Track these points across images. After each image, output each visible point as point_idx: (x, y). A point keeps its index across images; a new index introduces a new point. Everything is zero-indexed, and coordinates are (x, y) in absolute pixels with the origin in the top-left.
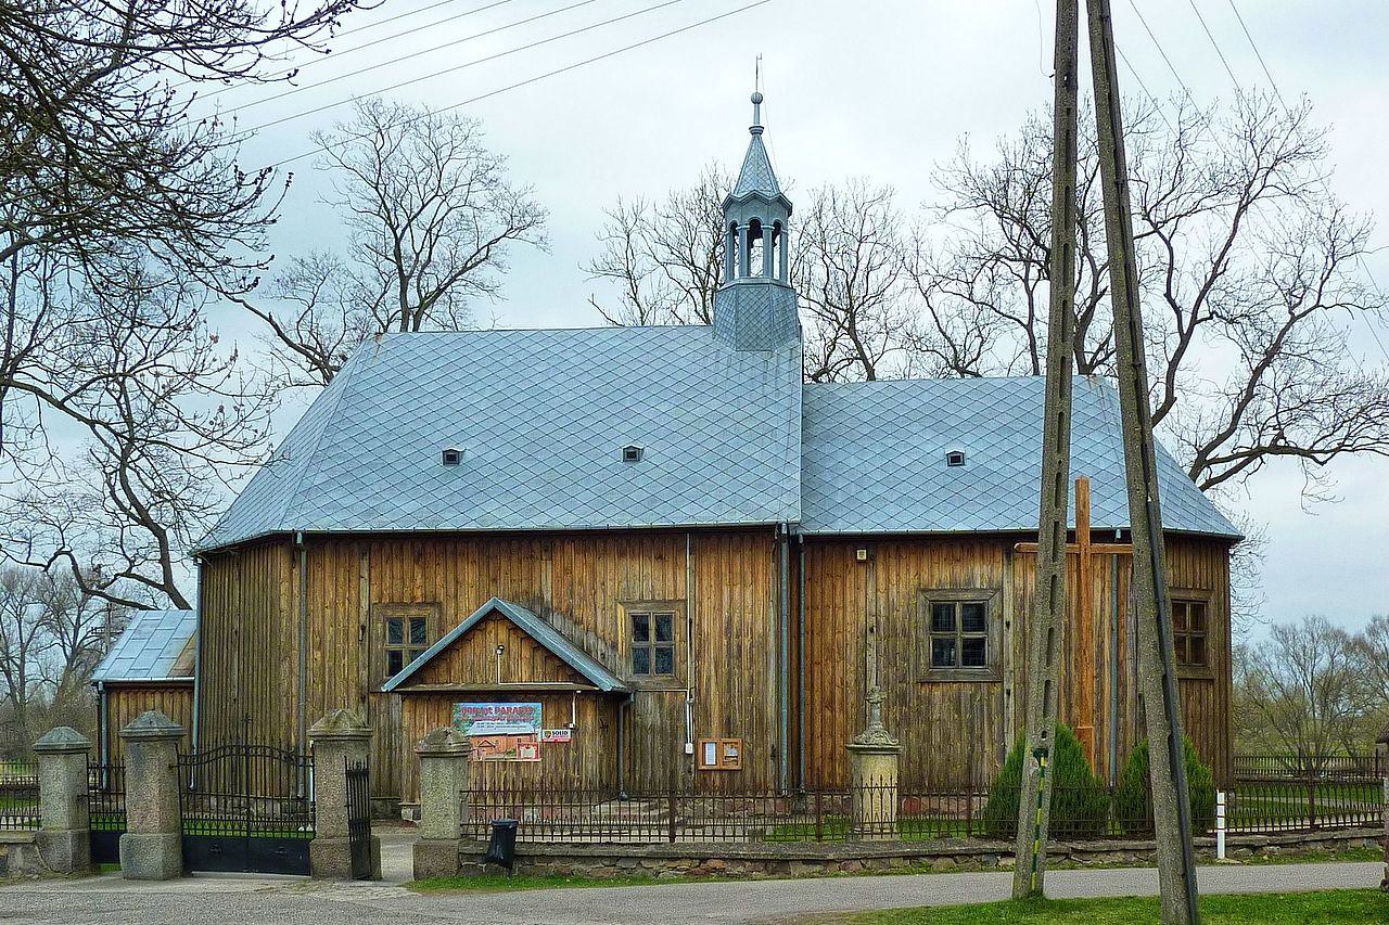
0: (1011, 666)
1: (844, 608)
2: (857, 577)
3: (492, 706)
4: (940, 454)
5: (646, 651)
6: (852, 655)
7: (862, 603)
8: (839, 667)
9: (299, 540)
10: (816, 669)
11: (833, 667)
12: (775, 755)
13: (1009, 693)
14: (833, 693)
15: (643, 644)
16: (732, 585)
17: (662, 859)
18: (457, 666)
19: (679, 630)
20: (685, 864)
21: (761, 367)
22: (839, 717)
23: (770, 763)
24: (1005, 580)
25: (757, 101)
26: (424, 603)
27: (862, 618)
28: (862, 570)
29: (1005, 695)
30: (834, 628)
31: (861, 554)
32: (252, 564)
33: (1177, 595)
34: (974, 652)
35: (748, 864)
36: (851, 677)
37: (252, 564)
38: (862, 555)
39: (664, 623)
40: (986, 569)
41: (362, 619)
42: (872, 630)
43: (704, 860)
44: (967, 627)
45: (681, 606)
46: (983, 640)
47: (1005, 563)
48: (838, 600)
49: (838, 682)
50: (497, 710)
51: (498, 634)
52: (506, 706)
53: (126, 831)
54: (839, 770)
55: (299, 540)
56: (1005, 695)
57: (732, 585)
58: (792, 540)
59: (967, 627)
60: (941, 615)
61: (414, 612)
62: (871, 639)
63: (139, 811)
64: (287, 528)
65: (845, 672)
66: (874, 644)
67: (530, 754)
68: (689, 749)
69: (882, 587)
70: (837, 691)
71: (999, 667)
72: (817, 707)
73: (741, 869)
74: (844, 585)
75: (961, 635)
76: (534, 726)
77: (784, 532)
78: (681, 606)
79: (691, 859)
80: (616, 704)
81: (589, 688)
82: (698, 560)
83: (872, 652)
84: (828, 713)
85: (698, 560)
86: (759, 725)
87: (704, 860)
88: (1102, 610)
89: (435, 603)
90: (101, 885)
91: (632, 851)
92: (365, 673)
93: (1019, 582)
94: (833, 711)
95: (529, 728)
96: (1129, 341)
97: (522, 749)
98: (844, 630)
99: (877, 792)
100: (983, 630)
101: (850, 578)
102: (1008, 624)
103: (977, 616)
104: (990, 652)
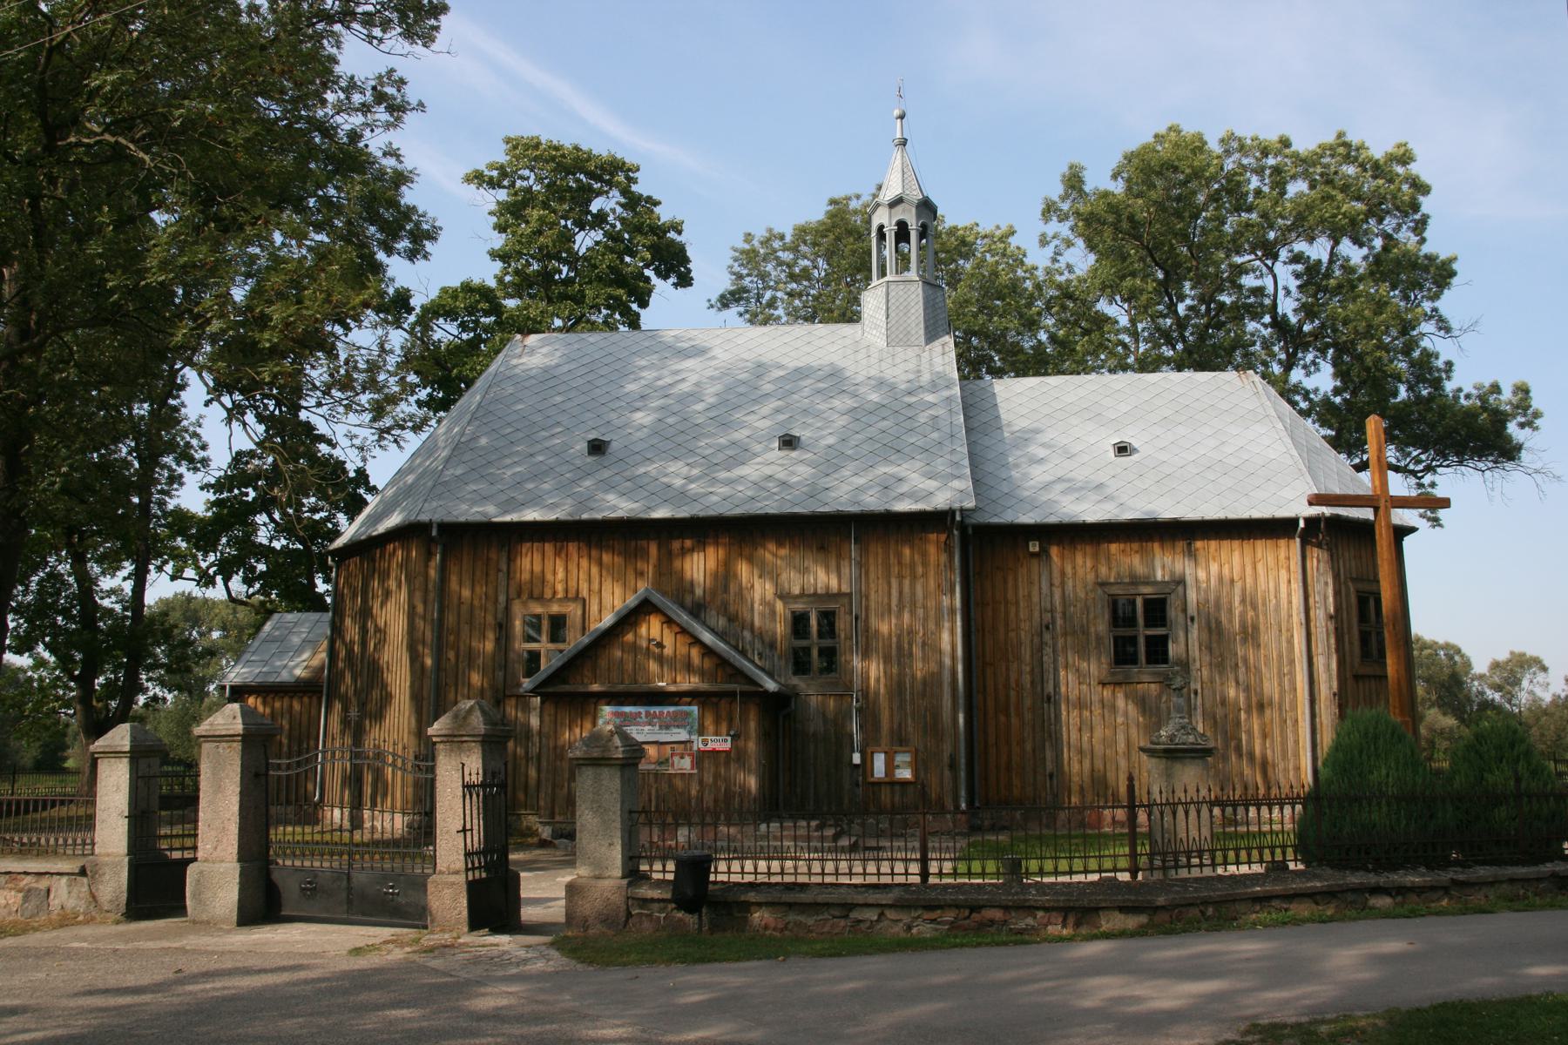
0: (1198, 664)
1: (1017, 603)
2: (1029, 571)
3: (642, 710)
5: (807, 650)
6: (1026, 654)
7: (1035, 599)
9: (434, 533)
10: (989, 671)
11: (1008, 669)
12: (953, 766)
14: (1008, 697)
15: (804, 643)
16: (901, 577)
17: (916, 908)
18: (603, 663)
19: (843, 624)
20: (949, 916)
21: (914, 361)
22: (1014, 720)
23: (947, 773)
26: (566, 598)
27: (1036, 614)
28: (1035, 562)
30: (1007, 625)
33: (1360, 586)
34: (1158, 651)
35: (1040, 914)
36: (1027, 679)
38: (1034, 547)
39: (828, 618)
40: (1168, 560)
41: (500, 616)
43: (975, 908)
44: (1149, 623)
45: (846, 600)
48: (1010, 595)
50: (648, 714)
51: (892, 286)
52: (657, 710)
53: (195, 859)
54: (1016, 782)
55: (434, 533)
57: (901, 577)
58: (963, 527)
59: (1149, 623)
60: (1121, 615)
61: (555, 609)
63: (213, 833)
64: (424, 518)
65: (1020, 673)
67: (685, 764)
68: (857, 758)
70: (1013, 694)
71: (1185, 665)
73: (1030, 921)
74: (1016, 580)
75: (1143, 632)
76: (690, 733)
77: (958, 518)
78: (846, 600)
79: (957, 907)
80: (778, 708)
81: (753, 688)
82: (864, 550)
84: (1002, 719)
85: (864, 550)
86: (932, 727)
87: (975, 908)
88: (1290, 602)
89: (577, 597)
90: (151, 936)
91: (873, 897)
92: (501, 674)
94: (1008, 716)
95: (683, 735)
97: (676, 759)
98: (1018, 628)
99: (1192, 808)
101: (1023, 572)
102: (1192, 619)
103: (1157, 610)
104: (1174, 650)
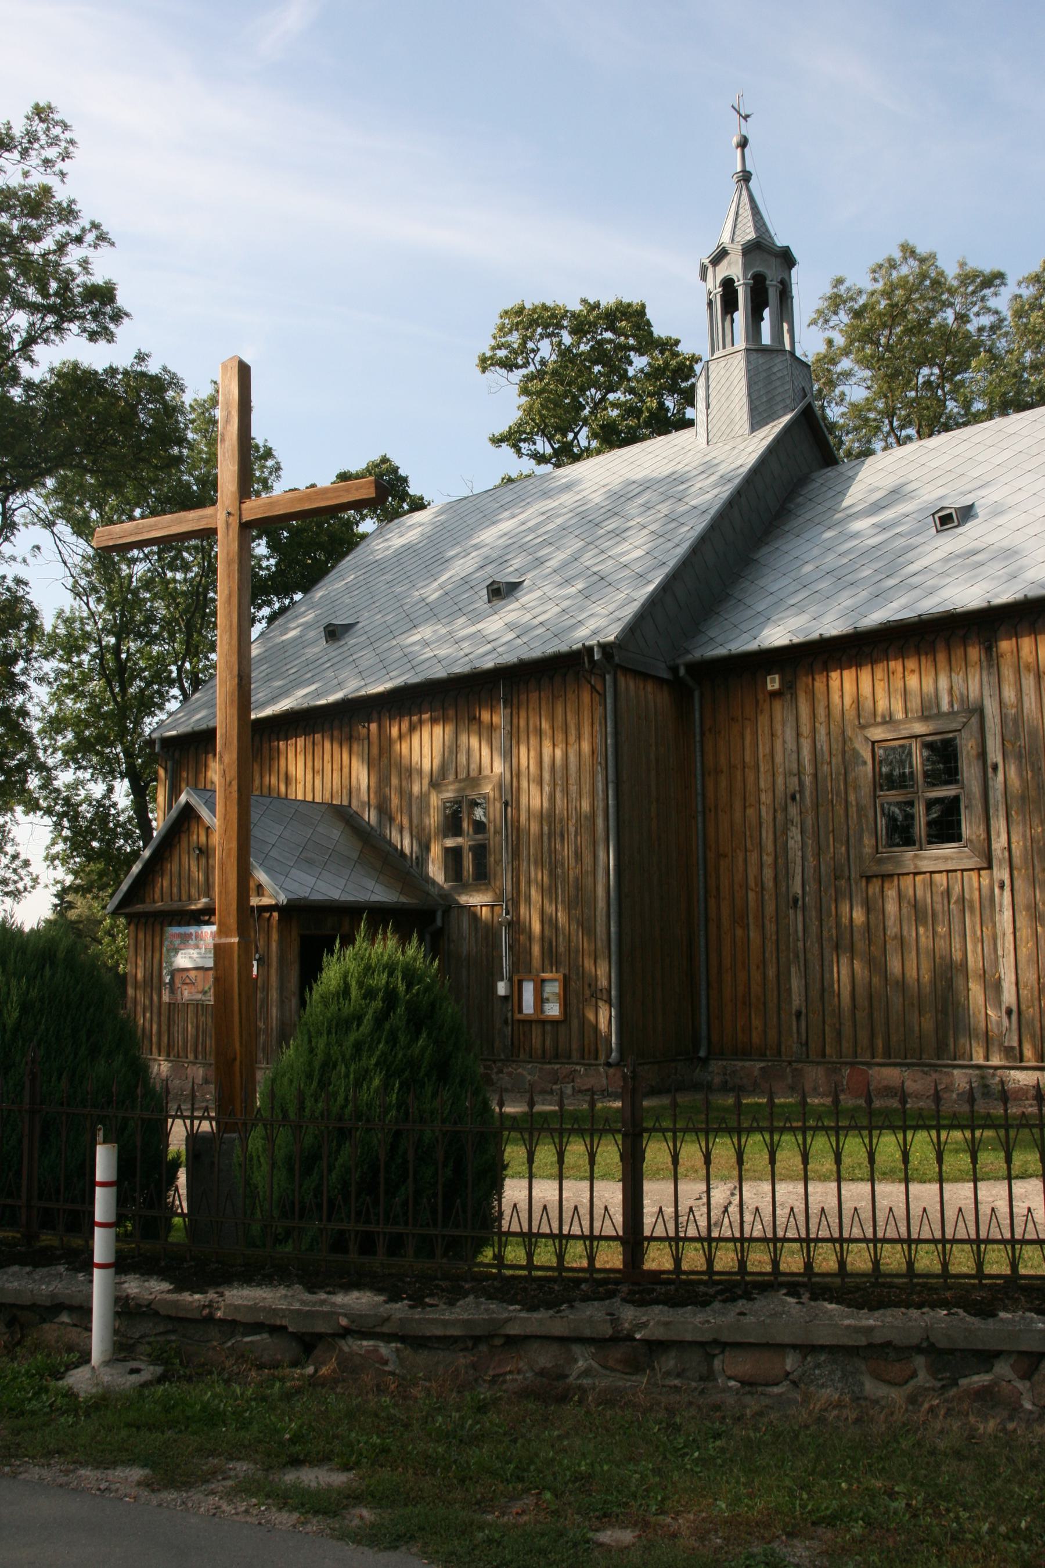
4: (526, 598)
8: (753, 858)
13: (1002, 886)
22: (754, 934)
24: (986, 693)
25: (743, 144)
28: (777, 705)
29: (997, 890)
31: (773, 681)
32: (327, 757)
37: (327, 757)
42: (793, 798)
44: (933, 779)
46: (956, 799)
47: (985, 664)
49: (752, 883)
56: (997, 890)
62: (793, 811)
66: (797, 819)
69: (805, 730)
72: (726, 923)
83: (795, 832)
93: (1009, 694)
96: (783, 1015)
100: (956, 782)
102: (995, 768)
